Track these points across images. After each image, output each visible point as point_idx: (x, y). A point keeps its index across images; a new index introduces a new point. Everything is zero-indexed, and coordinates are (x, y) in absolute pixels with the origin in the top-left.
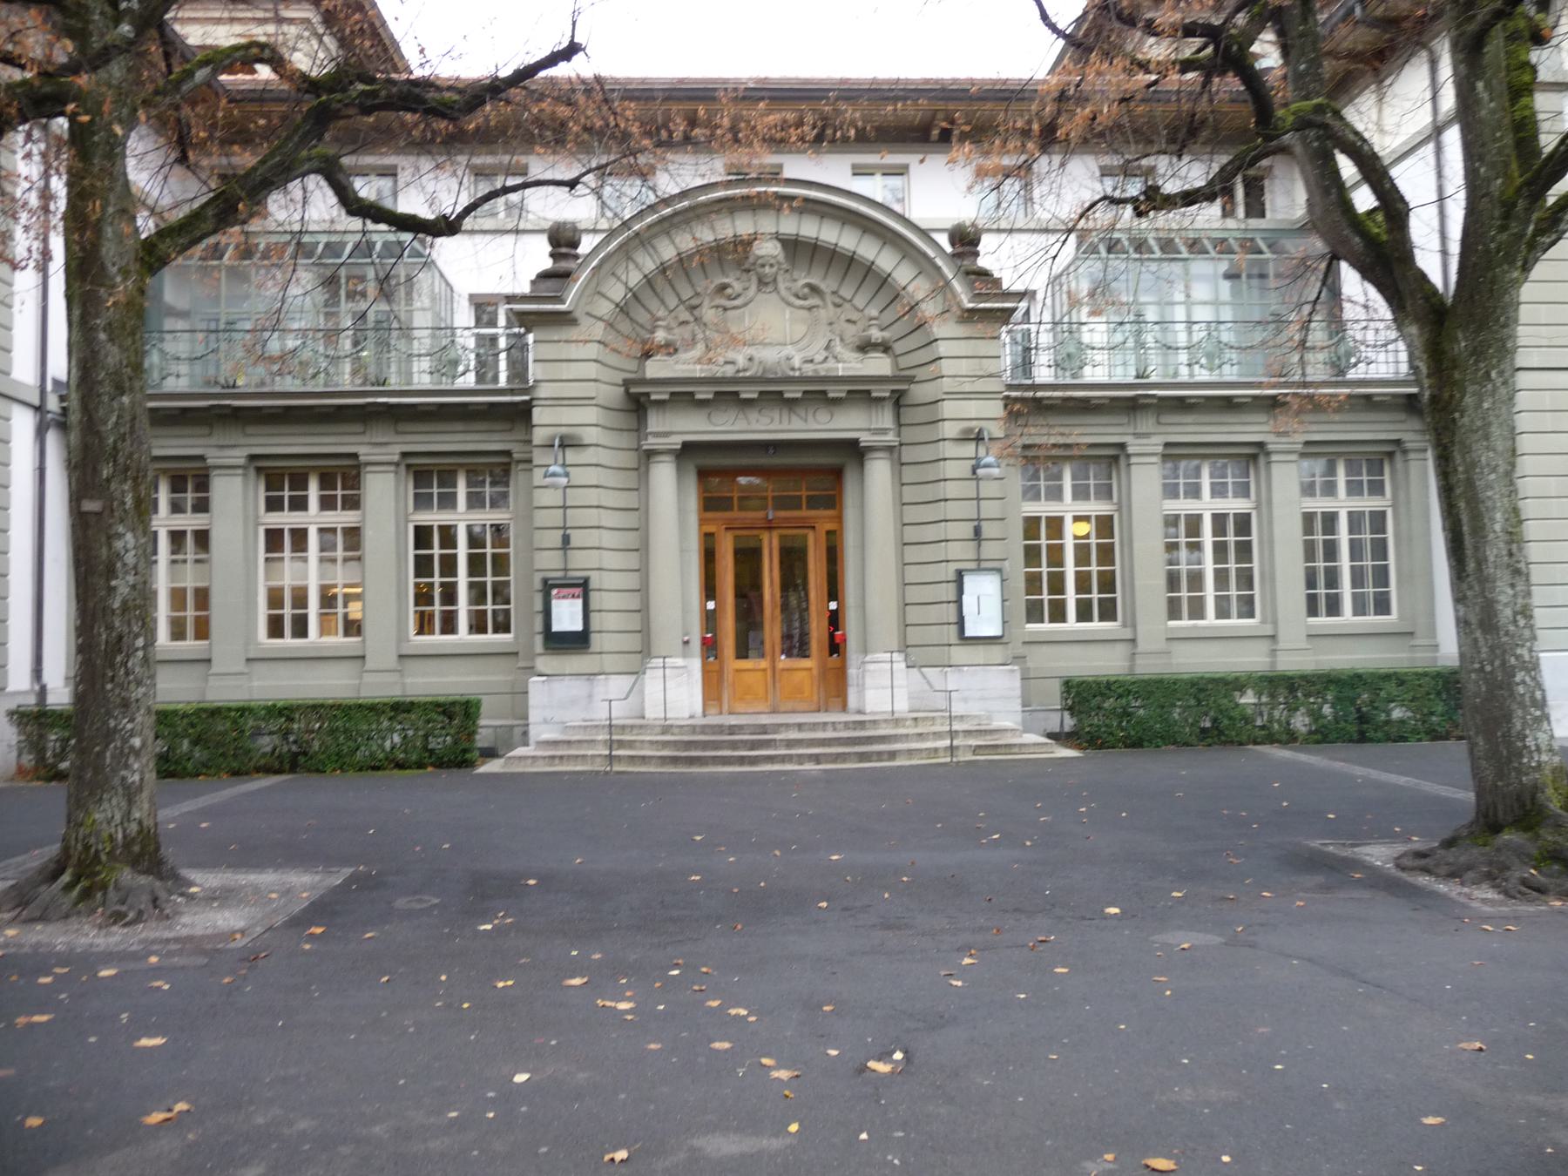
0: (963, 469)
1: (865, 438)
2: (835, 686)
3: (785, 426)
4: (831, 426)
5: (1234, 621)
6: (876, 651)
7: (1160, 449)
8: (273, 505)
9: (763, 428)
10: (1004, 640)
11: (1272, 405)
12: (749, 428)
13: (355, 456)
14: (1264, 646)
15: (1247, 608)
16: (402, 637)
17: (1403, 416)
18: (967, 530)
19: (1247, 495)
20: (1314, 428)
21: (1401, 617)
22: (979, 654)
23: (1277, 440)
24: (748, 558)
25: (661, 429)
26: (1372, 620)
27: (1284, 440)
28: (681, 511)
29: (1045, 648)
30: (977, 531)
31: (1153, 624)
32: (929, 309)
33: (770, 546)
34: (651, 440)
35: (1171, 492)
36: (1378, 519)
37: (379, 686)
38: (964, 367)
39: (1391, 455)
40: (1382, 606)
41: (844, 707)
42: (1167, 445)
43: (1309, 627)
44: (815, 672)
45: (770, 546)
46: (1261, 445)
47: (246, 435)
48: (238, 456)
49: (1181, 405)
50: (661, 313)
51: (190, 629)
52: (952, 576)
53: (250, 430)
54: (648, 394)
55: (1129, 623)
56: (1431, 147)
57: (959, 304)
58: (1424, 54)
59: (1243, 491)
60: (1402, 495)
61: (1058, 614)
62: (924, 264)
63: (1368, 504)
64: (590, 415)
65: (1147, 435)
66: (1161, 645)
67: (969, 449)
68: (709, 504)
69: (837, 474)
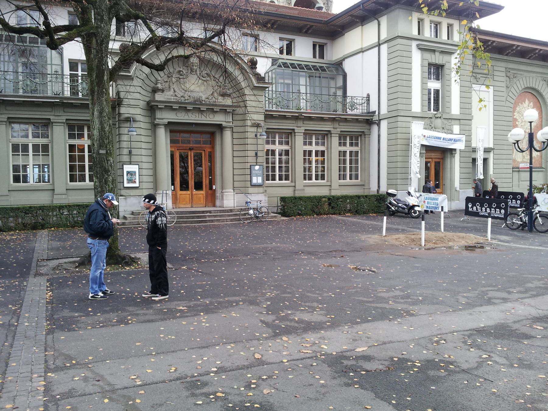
0: (253, 135)
1: (224, 124)
2: (212, 198)
3: (200, 119)
4: (214, 120)
5: (320, 181)
6: (226, 189)
7: (304, 131)
8: (71, 136)
9: (193, 119)
10: (139, 188)
11: (333, 120)
12: (189, 118)
13: (50, 119)
14: (328, 188)
15: (323, 178)
16: (67, 184)
17: (365, 125)
18: (253, 154)
19: (358, 146)
20: (343, 127)
21: (361, 181)
22: (256, 190)
23: (334, 130)
24: (184, 159)
25: (161, 117)
26: (354, 181)
27: (335, 130)
28: (166, 144)
29: (271, 188)
30: (256, 154)
31: (301, 182)
32: (243, 84)
33: (191, 155)
34: (157, 120)
35: (305, 144)
36: (357, 153)
37: (59, 200)
38: (254, 104)
39: (327, 134)
40: (357, 178)
41: (214, 206)
42: (305, 130)
43: (339, 183)
44: (205, 195)
45: (191, 155)
46: (329, 131)
47: (6, 110)
48: (63, 119)
49: (310, 119)
50: (159, 78)
51: (354, 177)
52: (249, 167)
53: (8, 108)
54: (157, 105)
55: (293, 181)
56: (377, 48)
57: (253, 84)
58: (376, 21)
59: (323, 144)
60: (363, 147)
61: (274, 179)
62: (242, 69)
63: (354, 149)
64: (138, 111)
65: (300, 127)
66: (302, 188)
67: (254, 129)
68: (172, 141)
69: (213, 134)
